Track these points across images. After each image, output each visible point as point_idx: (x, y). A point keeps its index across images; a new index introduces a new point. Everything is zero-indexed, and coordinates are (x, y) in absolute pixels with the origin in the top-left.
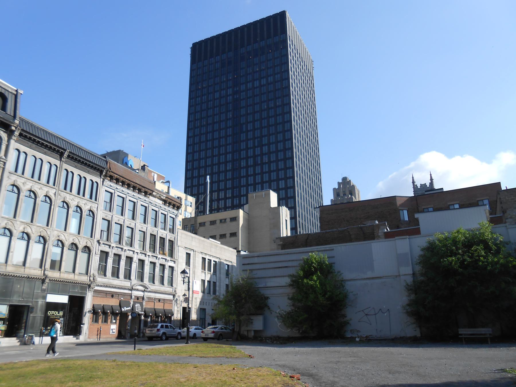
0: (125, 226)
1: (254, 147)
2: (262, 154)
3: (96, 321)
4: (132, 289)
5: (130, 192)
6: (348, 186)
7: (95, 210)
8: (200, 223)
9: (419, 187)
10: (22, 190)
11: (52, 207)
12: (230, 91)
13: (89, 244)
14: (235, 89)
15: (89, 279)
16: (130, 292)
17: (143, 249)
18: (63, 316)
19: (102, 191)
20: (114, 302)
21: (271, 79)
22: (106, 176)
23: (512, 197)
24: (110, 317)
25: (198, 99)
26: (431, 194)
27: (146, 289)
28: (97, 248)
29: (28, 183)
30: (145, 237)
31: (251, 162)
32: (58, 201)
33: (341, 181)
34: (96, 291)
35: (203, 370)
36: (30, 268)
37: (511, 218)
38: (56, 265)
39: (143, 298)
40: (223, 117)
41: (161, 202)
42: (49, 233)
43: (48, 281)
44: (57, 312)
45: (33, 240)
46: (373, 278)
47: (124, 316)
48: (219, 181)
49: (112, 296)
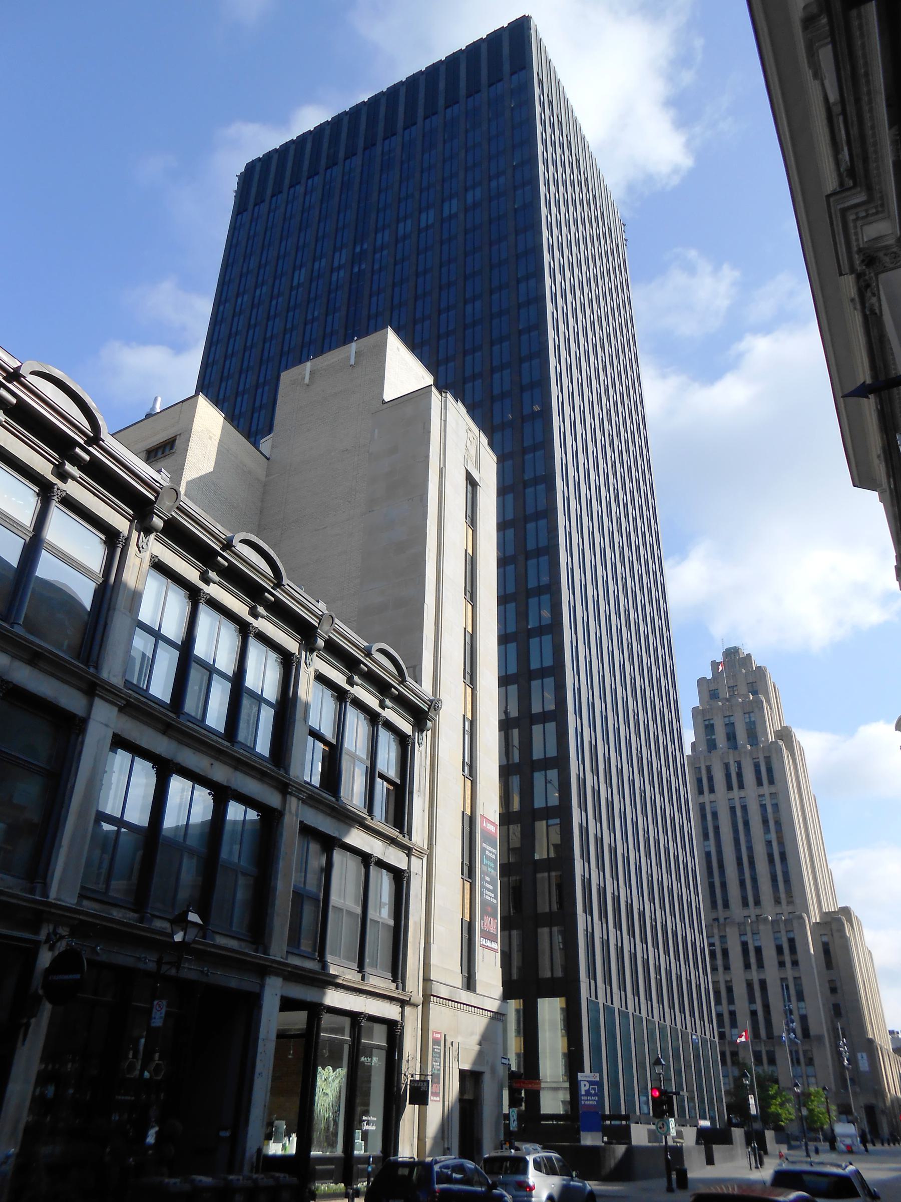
6: (744, 671)
33: (719, 658)
35: (379, 149)
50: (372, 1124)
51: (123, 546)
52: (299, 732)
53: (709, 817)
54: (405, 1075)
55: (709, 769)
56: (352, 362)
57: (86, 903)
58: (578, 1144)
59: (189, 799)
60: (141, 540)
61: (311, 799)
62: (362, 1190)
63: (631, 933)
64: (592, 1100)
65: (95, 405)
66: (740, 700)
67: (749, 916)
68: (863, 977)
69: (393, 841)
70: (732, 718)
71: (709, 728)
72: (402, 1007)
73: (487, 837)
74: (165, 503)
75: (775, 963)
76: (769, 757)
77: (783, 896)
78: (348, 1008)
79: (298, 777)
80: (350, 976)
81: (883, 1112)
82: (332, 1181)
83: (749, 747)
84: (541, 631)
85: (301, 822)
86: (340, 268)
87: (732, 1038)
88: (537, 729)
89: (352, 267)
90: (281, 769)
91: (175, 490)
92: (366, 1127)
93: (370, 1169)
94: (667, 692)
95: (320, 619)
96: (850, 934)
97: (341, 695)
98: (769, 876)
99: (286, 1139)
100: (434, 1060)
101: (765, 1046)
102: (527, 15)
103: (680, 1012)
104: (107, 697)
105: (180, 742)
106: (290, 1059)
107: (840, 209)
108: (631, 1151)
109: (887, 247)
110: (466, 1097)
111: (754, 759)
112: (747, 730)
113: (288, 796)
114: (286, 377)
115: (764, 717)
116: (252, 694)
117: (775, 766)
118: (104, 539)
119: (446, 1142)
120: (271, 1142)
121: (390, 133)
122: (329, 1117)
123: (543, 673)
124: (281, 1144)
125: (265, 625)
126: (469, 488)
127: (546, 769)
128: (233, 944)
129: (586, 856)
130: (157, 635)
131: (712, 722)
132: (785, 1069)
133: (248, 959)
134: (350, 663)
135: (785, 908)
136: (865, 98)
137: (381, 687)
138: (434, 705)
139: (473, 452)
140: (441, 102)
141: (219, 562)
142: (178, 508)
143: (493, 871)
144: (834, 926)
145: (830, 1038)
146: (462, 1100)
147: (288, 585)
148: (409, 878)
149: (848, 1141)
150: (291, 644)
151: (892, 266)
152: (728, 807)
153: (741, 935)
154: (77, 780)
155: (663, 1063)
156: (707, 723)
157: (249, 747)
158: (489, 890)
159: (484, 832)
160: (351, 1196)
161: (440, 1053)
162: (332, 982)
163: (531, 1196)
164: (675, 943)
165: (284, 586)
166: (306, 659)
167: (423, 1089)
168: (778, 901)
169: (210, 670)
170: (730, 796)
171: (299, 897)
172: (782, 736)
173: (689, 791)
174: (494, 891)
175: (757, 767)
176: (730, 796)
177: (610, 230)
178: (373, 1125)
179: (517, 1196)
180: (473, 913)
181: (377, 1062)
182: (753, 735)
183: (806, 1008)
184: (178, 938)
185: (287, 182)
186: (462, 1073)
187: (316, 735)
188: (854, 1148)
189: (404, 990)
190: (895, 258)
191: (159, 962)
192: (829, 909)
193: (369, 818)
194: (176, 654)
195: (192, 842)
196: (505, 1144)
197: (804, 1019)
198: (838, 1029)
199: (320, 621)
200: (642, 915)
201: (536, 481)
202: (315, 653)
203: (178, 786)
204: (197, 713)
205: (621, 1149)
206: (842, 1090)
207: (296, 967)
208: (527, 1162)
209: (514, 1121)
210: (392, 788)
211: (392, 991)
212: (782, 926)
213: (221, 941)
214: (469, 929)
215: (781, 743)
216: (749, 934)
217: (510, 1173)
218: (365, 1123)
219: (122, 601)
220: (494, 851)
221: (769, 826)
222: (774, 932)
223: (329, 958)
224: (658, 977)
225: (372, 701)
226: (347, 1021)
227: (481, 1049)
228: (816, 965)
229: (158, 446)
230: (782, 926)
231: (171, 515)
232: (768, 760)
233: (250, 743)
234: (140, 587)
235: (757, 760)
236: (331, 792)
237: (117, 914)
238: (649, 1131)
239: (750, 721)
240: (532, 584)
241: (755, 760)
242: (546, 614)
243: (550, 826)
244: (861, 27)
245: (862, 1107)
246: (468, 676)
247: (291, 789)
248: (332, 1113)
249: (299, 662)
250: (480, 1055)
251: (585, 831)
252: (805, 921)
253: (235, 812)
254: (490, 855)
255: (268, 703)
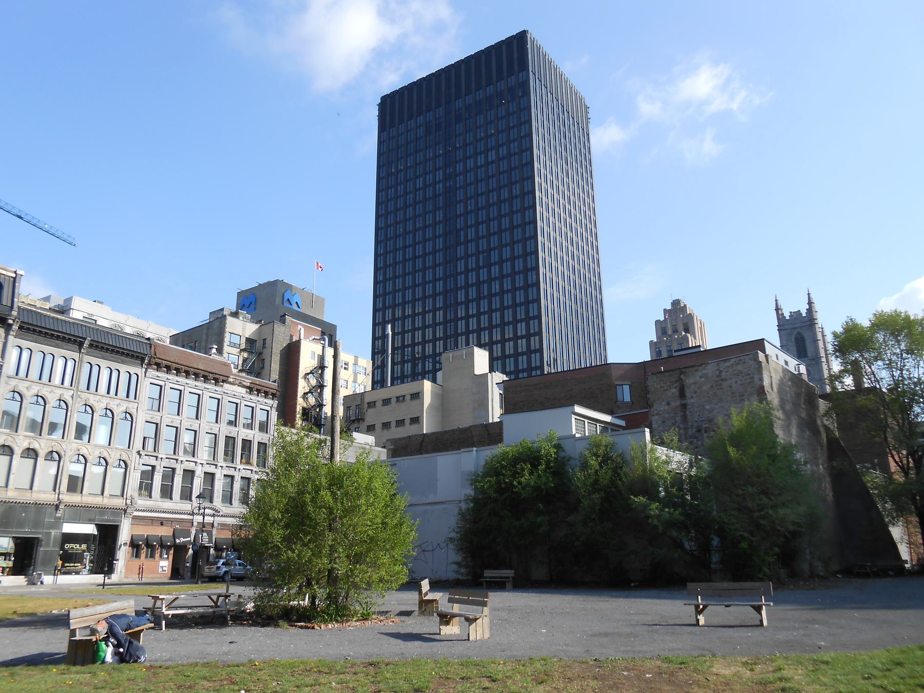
0: (183, 428)
1: (478, 268)
2: (490, 280)
3: (137, 556)
4: (193, 512)
5: (191, 382)
6: (681, 316)
7: (134, 412)
8: (368, 403)
9: (788, 318)
10: (25, 397)
11: (69, 413)
12: (440, 175)
13: (124, 456)
14: (448, 172)
15: (124, 503)
16: (191, 517)
17: (214, 459)
19: (145, 385)
20: (165, 532)
21: (503, 151)
22: (149, 364)
23: (662, 385)
24: (159, 550)
26: (687, 354)
27: (216, 513)
28: (137, 462)
29: (33, 387)
30: (217, 441)
31: (473, 293)
32: (77, 405)
33: (669, 307)
34: (135, 518)
36: (39, 492)
37: (657, 414)
38: (75, 484)
39: (212, 525)
40: (429, 219)
41: (244, 390)
42: (64, 447)
43: (63, 507)
44: (78, 546)
45: (41, 457)
46: (435, 503)
47: (179, 551)
48: (404, 332)
49: (162, 524)
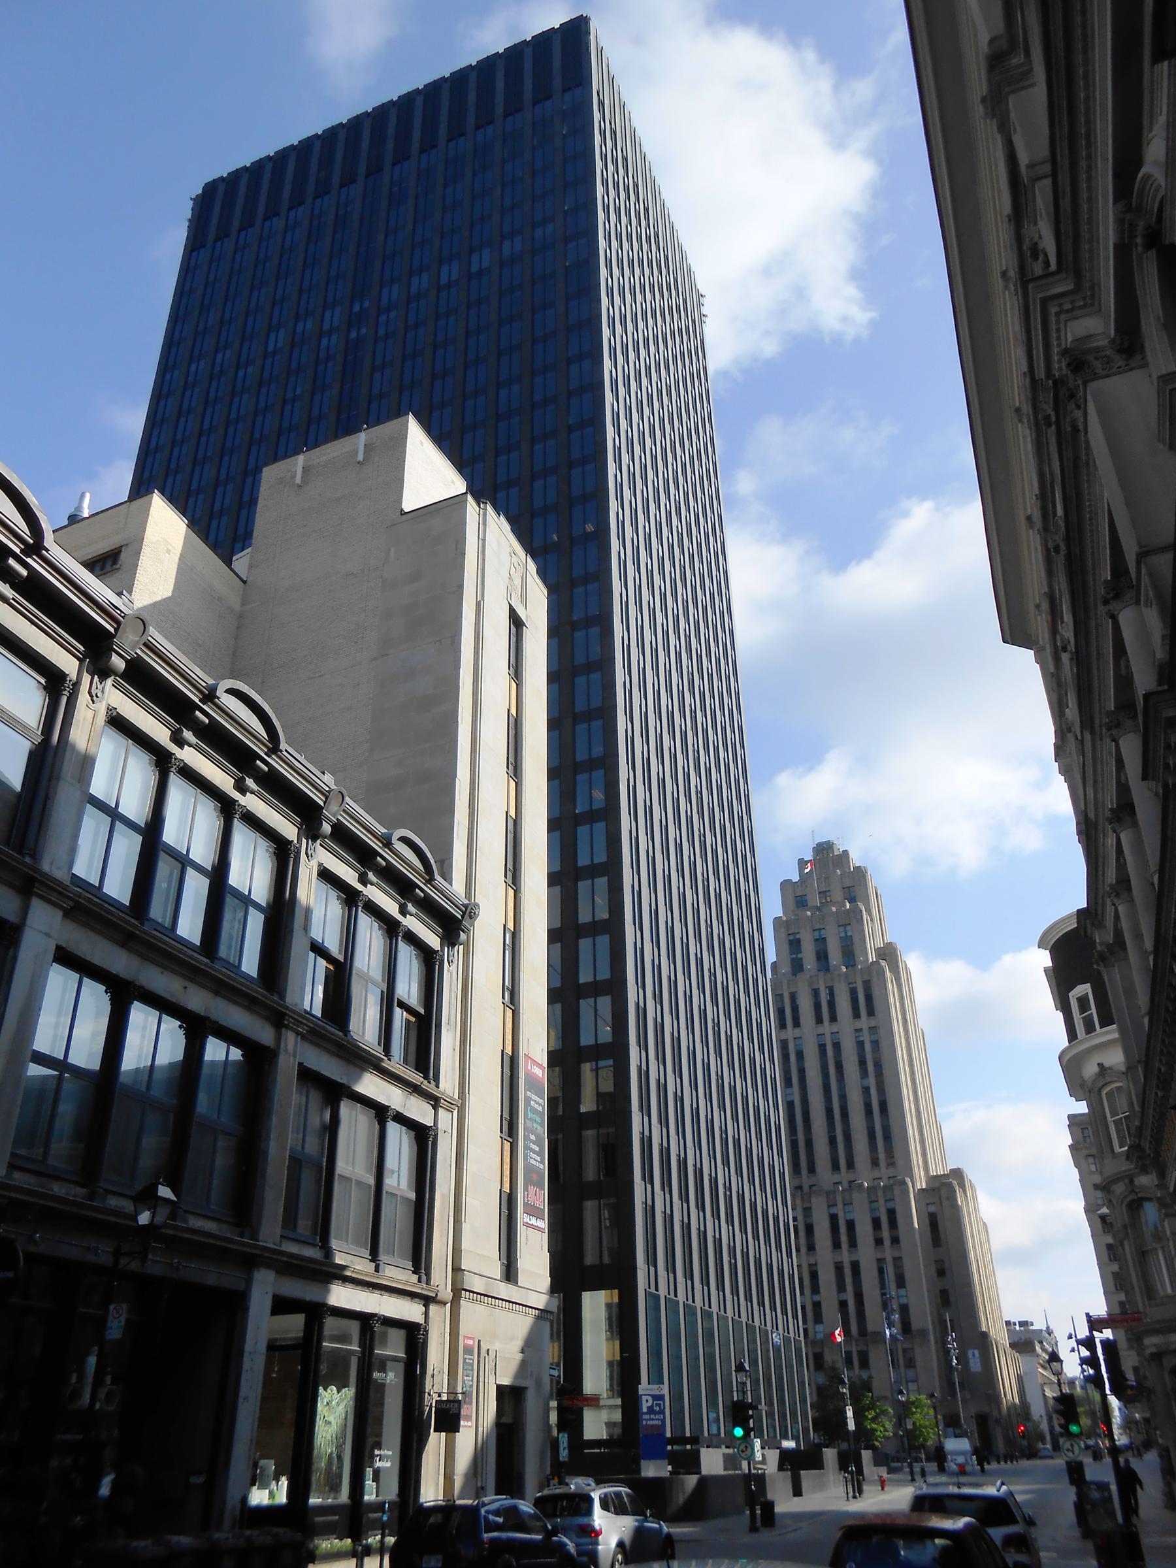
6: (839, 872)
18: (1090, 1375)
25: (224, 355)
33: (809, 856)
50: (386, 1460)
51: (70, 694)
52: (298, 945)
53: (793, 1058)
54: (429, 1394)
55: (793, 997)
56: (360, 457)
57: (17, 1175)
58: (637, 1476)
59: (67, 1034)
60: (94, 685)
61: (313, 1034)
62: (374, 1546)
63: (701, 1206)
64: (657, 1419)
65: (36, 502)
66: (834, 909)
67: (881, 1178)
68: (977, 1256)
69: (416, 1089)
70: (823, 932)
71: (795, 944)
72: (426, 1306)
73: (532, 1083)
74: (128, 637)
75: (871, 1240)
76: (869, 981)
77: (882, 1156)
78: (358, 1309)
79: (296, 1005)
80: (360, 1266)
81: (997, 1421)
82: (335, 1536)
83: (844, 969)
84: (592, 817)
85: (300, 1064)
86: (331, 331)
87: (815, 1336)
88: (585, 944)
89: (348, 332)
90: (275, 994)
91: (141, 619)
92: (378, 1464)
93: (385, 1518)
94: (748, 897)
95: (326, 796)
96: (962, 1202)
97: (350, 897)
98: (866, 1132)
99: (273, 1485)
100: (465, 1374)
101: (857, 1345)
102: (584, 15)
103: (759, 1305)
104: (49, 897)
105: (144, 958)
106: (275, 1378)
107: (1040, 298)
108: (704, 1482)
109: (1098, 350)
110: (504, 1420)
111: (849, 984)
112: (842, 946)
113: (284, 1030)
114: (270, 474)
115: (864, 931)
116: (237, 894)
117: (876, 993)
118: (44, 683)
119: (479, 1478)
120: (255, 1488)
121: (402, 156)
122: (331, 1454)
123: (593, 871)
124: (267, 1491)
125: (254, 803)
126: (513, 629)
127: (596, 995)
128: (210, 1226)
129: (645, 1109)
130: (113, 814)
131: (798, 937)
132: (882, 1374)
133: (232, 1246)
134: (362, 855)
135: (884, 1171)
136: (1083, 164)
137: (402, 886)
138: (470, 911)
139: (518, 582)
140: (471, 120)
141: (197, 718)
142: (145, 645)
143: (539, 1128)
144: (943, 1192)
145: (935, 1333)
146: (499, 1424)
147: (286, 751)
148: (436, 1136)
149: (961, 1460)
150: (288, 829)
151: (1104, 373)
152: (816, 1046)
153: (829, 1206)
154: (7, 1009)
155: (748, 1369)
156: (791, 937)
157: (233, 965)
158: (534, 1152)
159: (530, 1076)
160: (360, 1555)
161: (472, 1365)
162: (339, 1275)
163: (597, 1543)
164: (754, 1214)
165: (281, 751)
166: (307, 849)
167: (453, 1411)
168: (875, 1163)
169: (183, 861)
170: (820, 1030)
171: (296, 1162)
172: (885, 954)
173: (770, 1025)
174: (540, 1154)
175: (853, 993)
176: (820, 1030)
177: (685, 301)
178: (387, 1461)
179: (583, 1544)
180: (514, 1180)
181: (392, 1378)
182: (849, 954)
183: (907, 1296)
184: (144, 1218)
185: (261, 211)
186: (500, 1388)
187: (318, 949)
188: (968, 1468)
189: (428, 1283)
190: (1108, 363)
191: (117, 1254)
192: (937, 1172)
193: (386, 1058)
194: (139, 839)
195: (157, 1092)
196: (553, 1479)
197: (904, 1309)
198: (946, 1321)
199: (326, 799)
200: (714, 1182)
201: (588, 623)
202: (319, 842)
203: (140, 1017)
204: (164, 916)
205: (691, 1481)
206: (949, 1398)
207: (292, 1256)
208: (590, 1500)
209: (564, 1449)
210: (413, 1019)
211: (413, 1285)
212: (880, 1194)
213: (196, 1223)
214: (509, 1202)
215: (883, 963)
216: (840, 1206)
217: (567, 1516)
218: (378, 1458)
219: (68, 768)
220: (541, 1101)
221: (866, 1068)
222: (871, 1202)
223: (334, 1244)
224: (733, 1261)
225: (389, 905)
226: (354, 1327)
227: (524, 1357)
228: (921, 1241)
229: (94, 559)
230: (880, 1194)
231: (136, 653)
232: (867, 985)
233: (233, 959)
234: (92, 750)
235: (854, 985)
236: (336, 1025)
237: (58, 1189)
238: (726, 1456)
239: (846, 936)
240: (581, 756)
241: (851, 986)
242: (598, 795)
243: (600, 1068)
244: (1086, 76)
245: (972, 1416)
246: (509, 874)
247: (287, 1020)
248: (336, 1448)
249: (298, 854)
250: (523, 1364)
251: (644, 1076)
252: (908, 1187)
253: (215, 1050)
254: (536, 1106)
255: (257, 906)
